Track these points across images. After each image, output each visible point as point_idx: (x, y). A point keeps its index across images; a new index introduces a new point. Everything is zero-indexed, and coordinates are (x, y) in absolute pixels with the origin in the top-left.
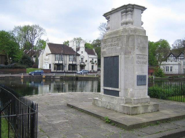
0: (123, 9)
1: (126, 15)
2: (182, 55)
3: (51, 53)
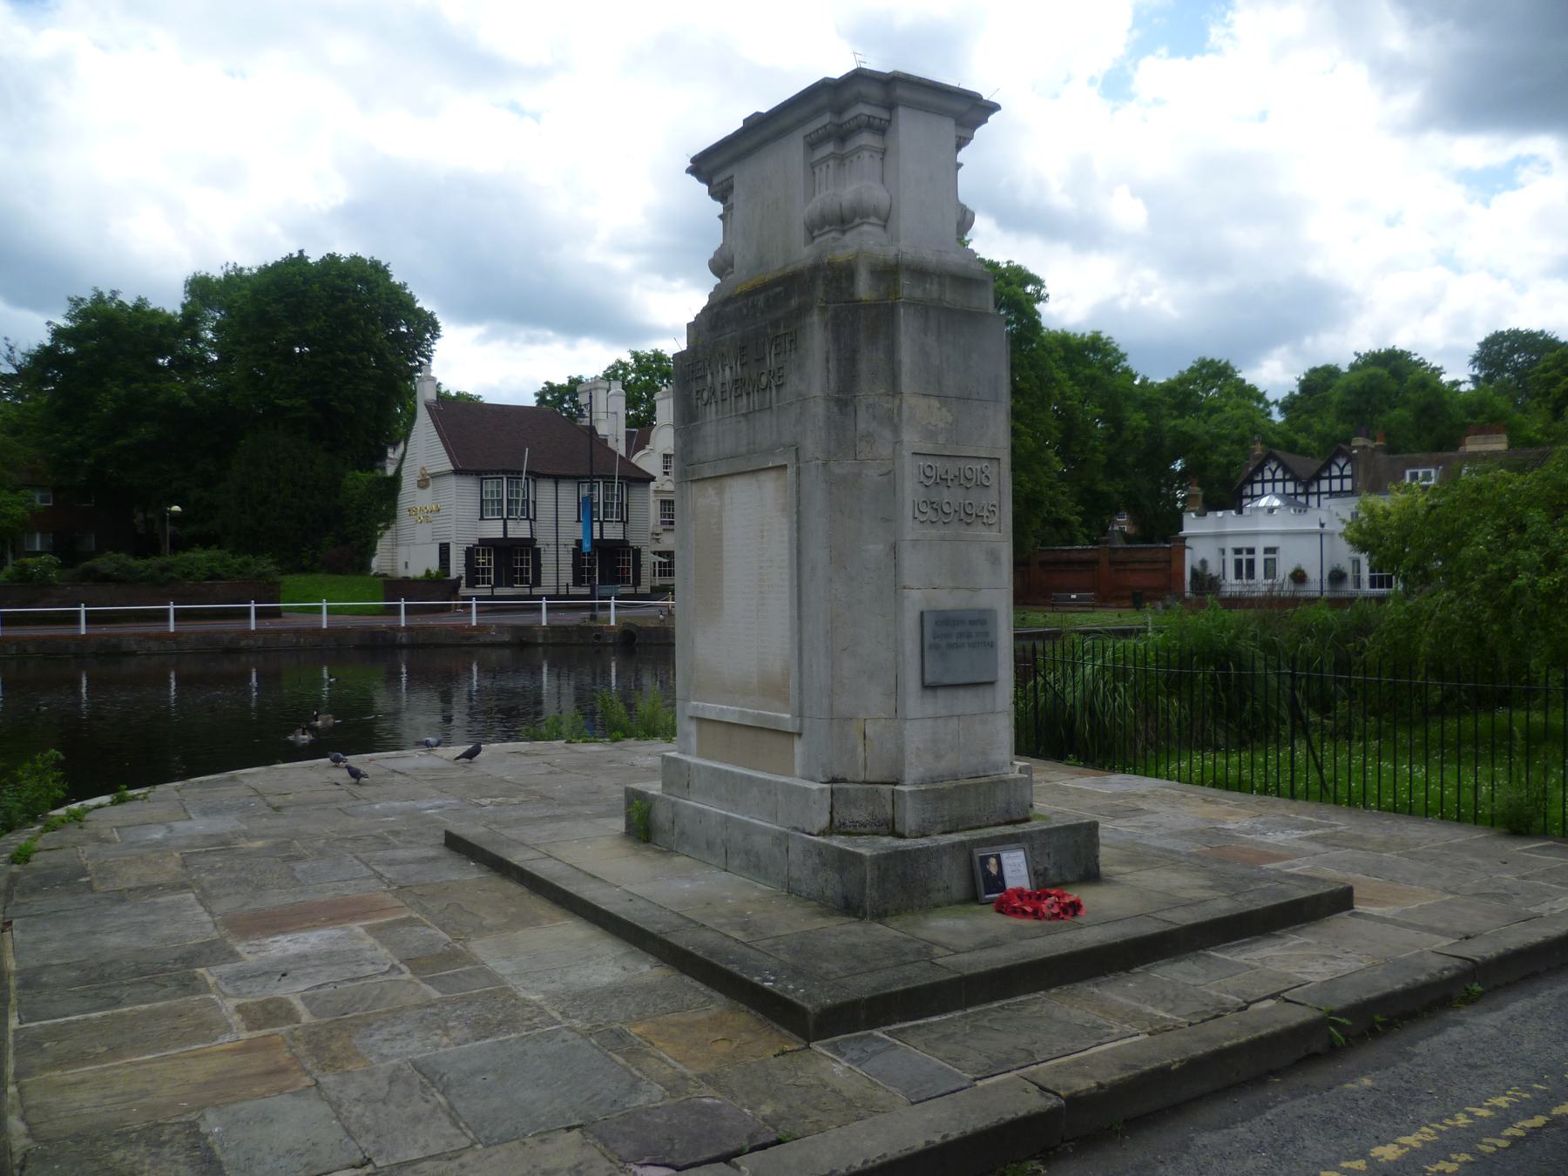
0: (818, 113)
1: (841, 159)
2: (1342, 470)
3: (448, 466)
